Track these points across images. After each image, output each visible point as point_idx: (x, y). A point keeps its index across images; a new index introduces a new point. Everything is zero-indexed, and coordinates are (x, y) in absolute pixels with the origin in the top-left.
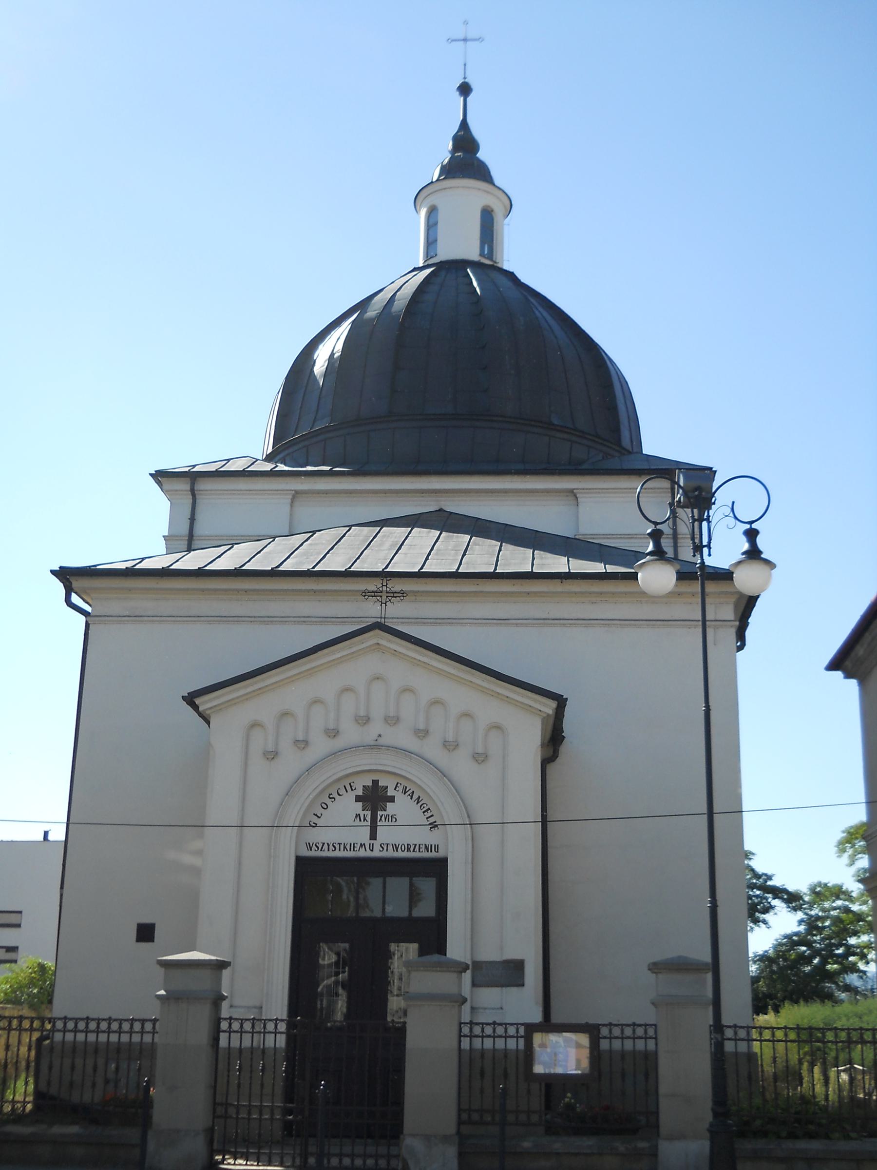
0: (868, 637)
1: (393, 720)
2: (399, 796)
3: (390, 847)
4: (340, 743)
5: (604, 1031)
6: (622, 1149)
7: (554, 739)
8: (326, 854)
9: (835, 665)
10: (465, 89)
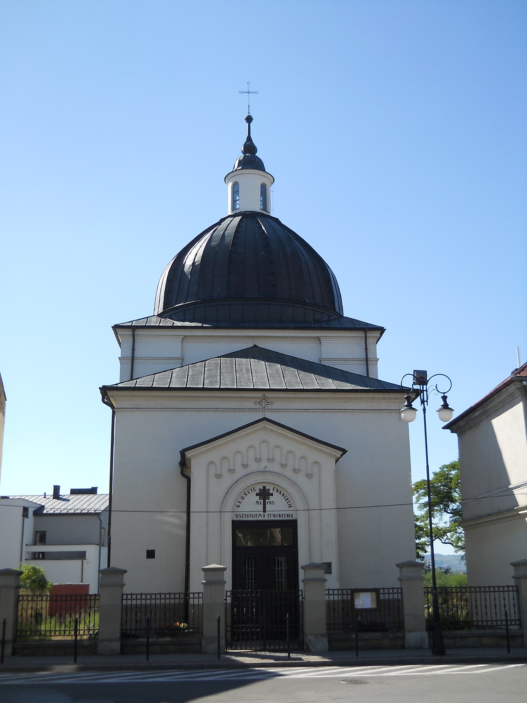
0: (466, 419)
1: (270, 460)
2: (275, 494)
3: (272, 515)
4: (248, 470)
5: (382, 591)
6: (391, 636)
8: (244, 519)
10: (249, 119)
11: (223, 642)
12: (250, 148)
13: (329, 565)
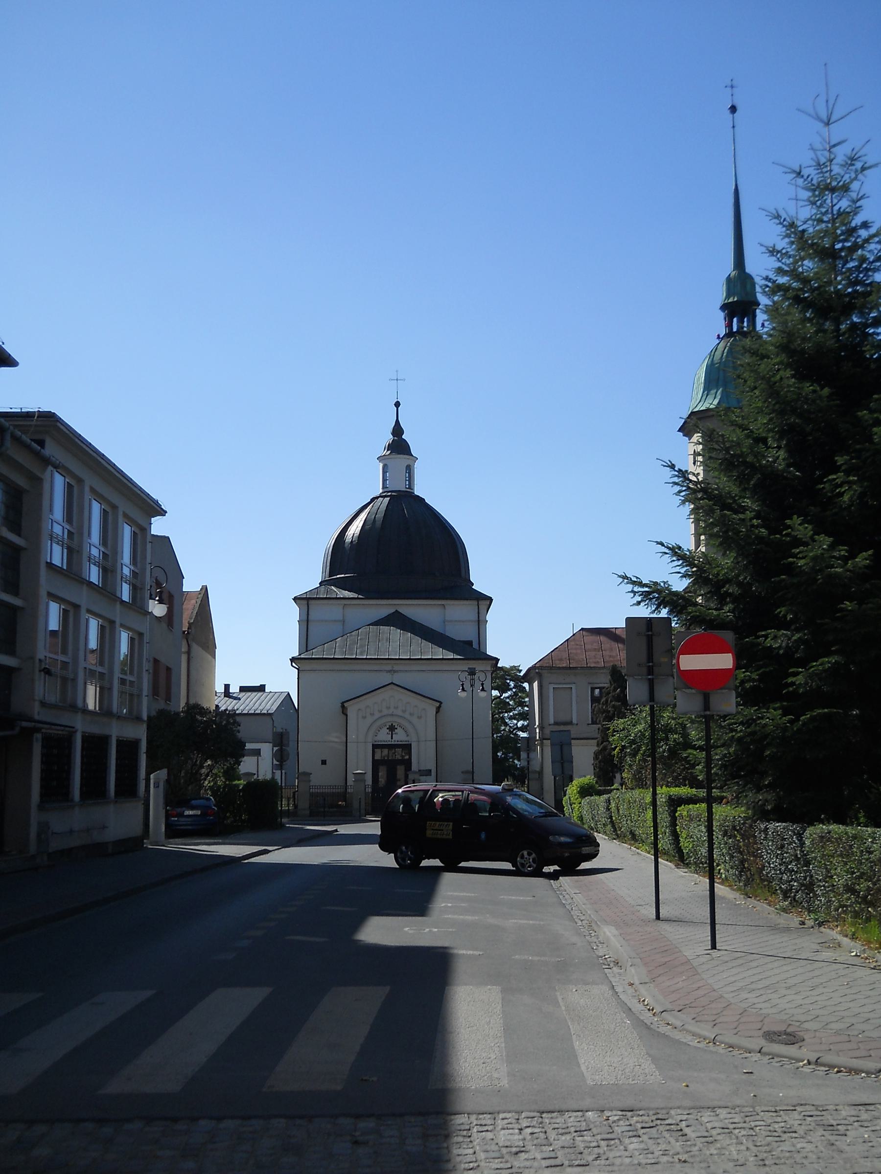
1: (396, 708)
4: (383, 714)
7: (438, 710)
9: (679, 431)
10: (397, 404)
11: (363, 812)
12: (398, 430)
13: (430, 771)
